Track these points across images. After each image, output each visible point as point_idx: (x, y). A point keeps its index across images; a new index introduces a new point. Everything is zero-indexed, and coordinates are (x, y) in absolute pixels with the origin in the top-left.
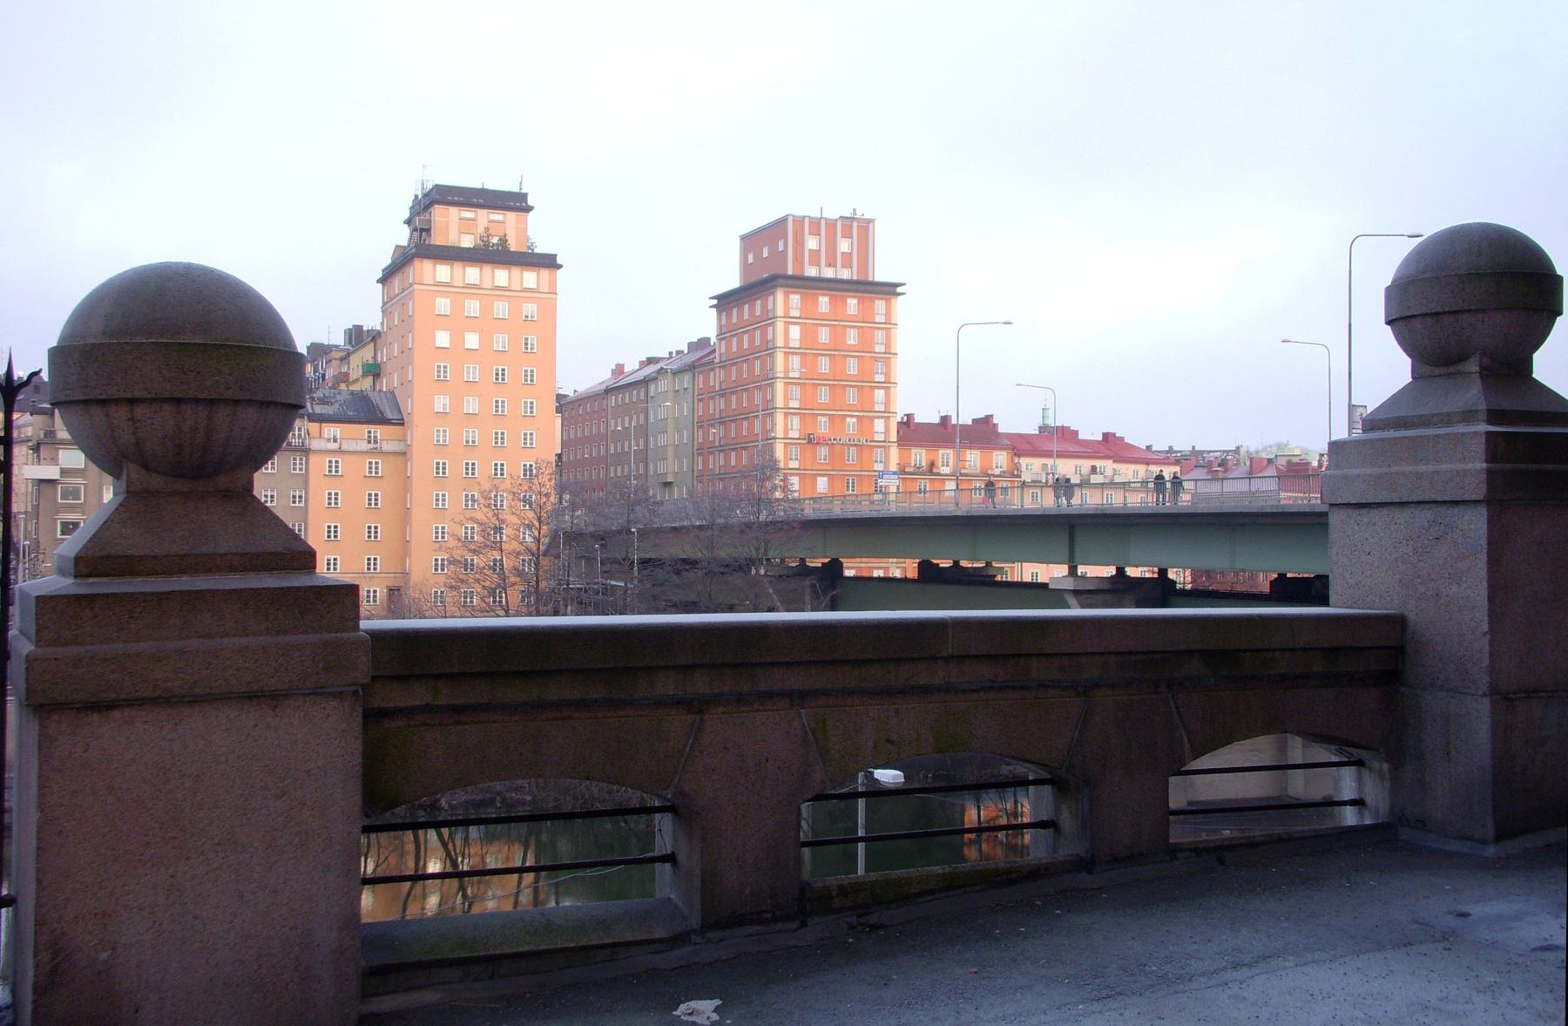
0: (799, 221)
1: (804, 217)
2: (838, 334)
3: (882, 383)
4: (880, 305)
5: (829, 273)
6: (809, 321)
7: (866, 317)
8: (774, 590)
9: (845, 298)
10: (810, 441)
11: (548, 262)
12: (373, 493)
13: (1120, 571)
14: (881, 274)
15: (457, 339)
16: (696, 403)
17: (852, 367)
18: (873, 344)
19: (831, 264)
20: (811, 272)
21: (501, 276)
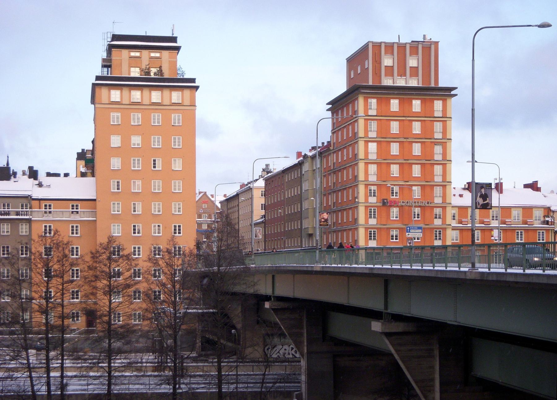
0: (377, 46)
1: (381, 43)
2: (406, 127)
3: (441, 161)
4: (438, 105)
5: (401, 82)
9: (432, 101)
10: (384, 204)
12: (137, 247)
14: (441, 84)
16: (323, 178)
17: (417, 149)
18: (433, 132)
19: (402, 73)
20: (387, 82)
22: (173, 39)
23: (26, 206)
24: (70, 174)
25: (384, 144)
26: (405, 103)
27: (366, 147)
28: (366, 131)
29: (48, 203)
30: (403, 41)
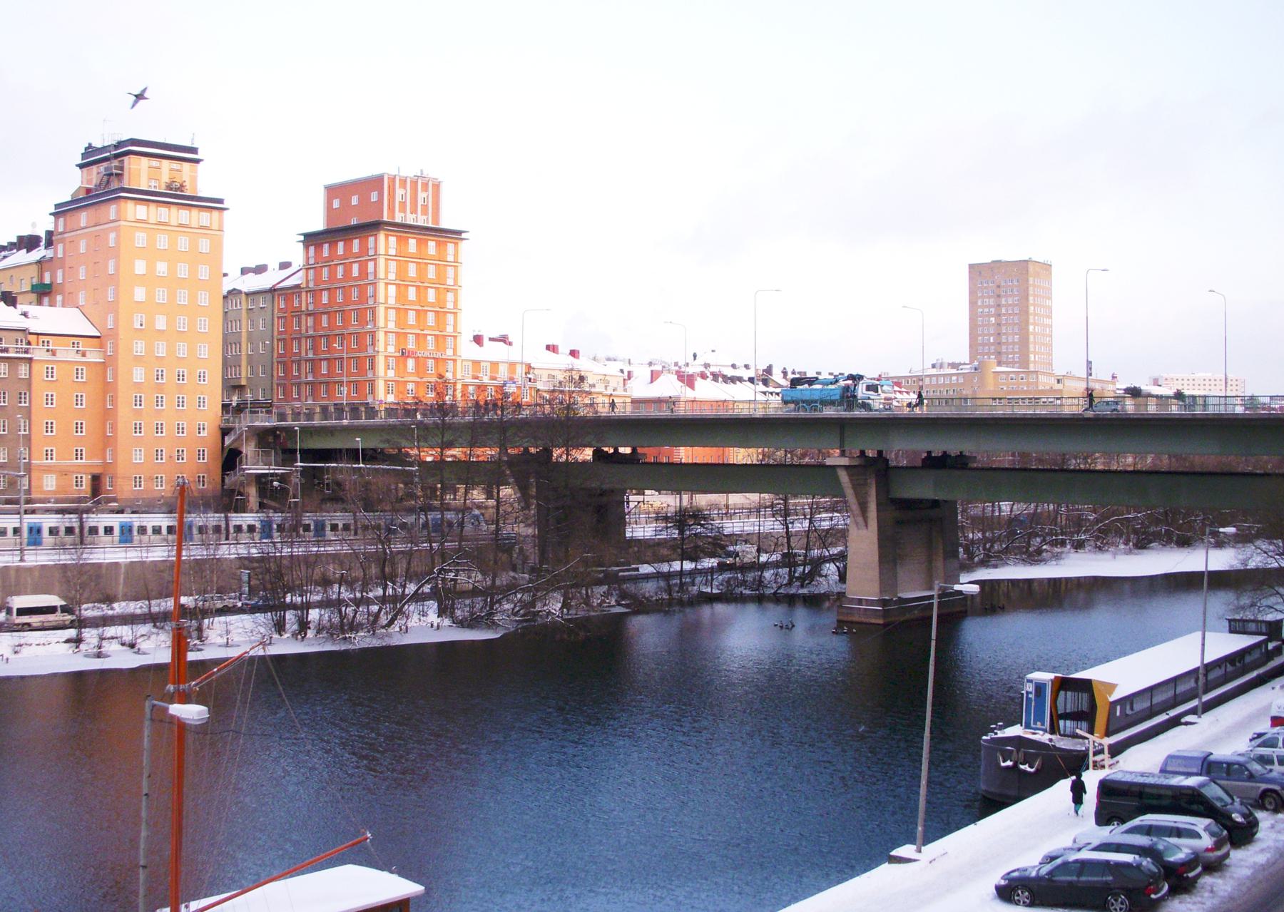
1: (395, 176)
6: (402, 257)
7: (441, 257)
8: (511, 472)
11: (214, 205)
13: (616, 450)
14: (444, 224)
15: (151, 268)
18: (445, 278)
20: (398, 218)
21: (184, 216)
22: (194, 150)
23: (21, 341)
24: (475, 334)
25: (402, 288)
26: (421, 244)
27: (386, 289)
28: (387, 272)
29: (46, 339)
30: (403, 174)
